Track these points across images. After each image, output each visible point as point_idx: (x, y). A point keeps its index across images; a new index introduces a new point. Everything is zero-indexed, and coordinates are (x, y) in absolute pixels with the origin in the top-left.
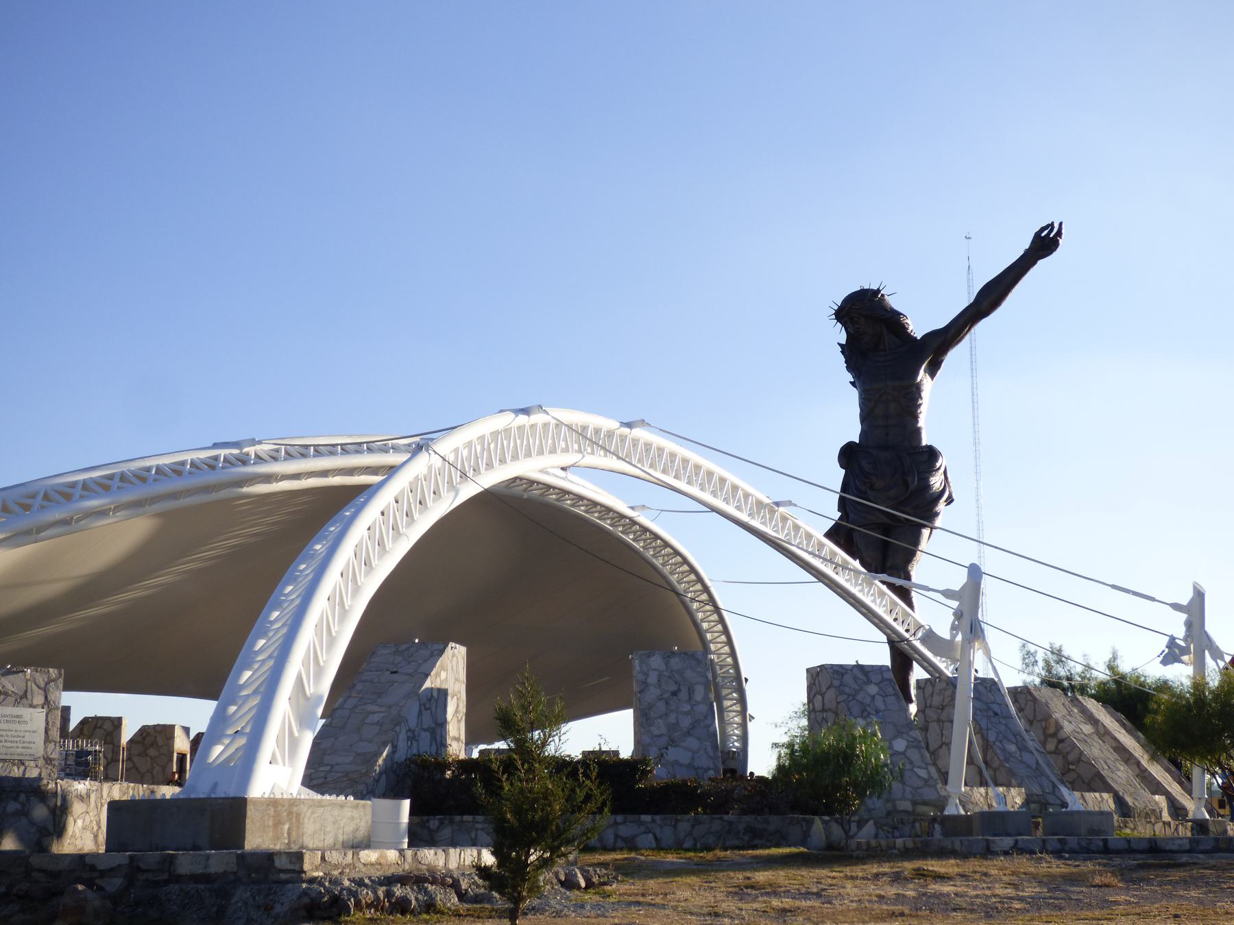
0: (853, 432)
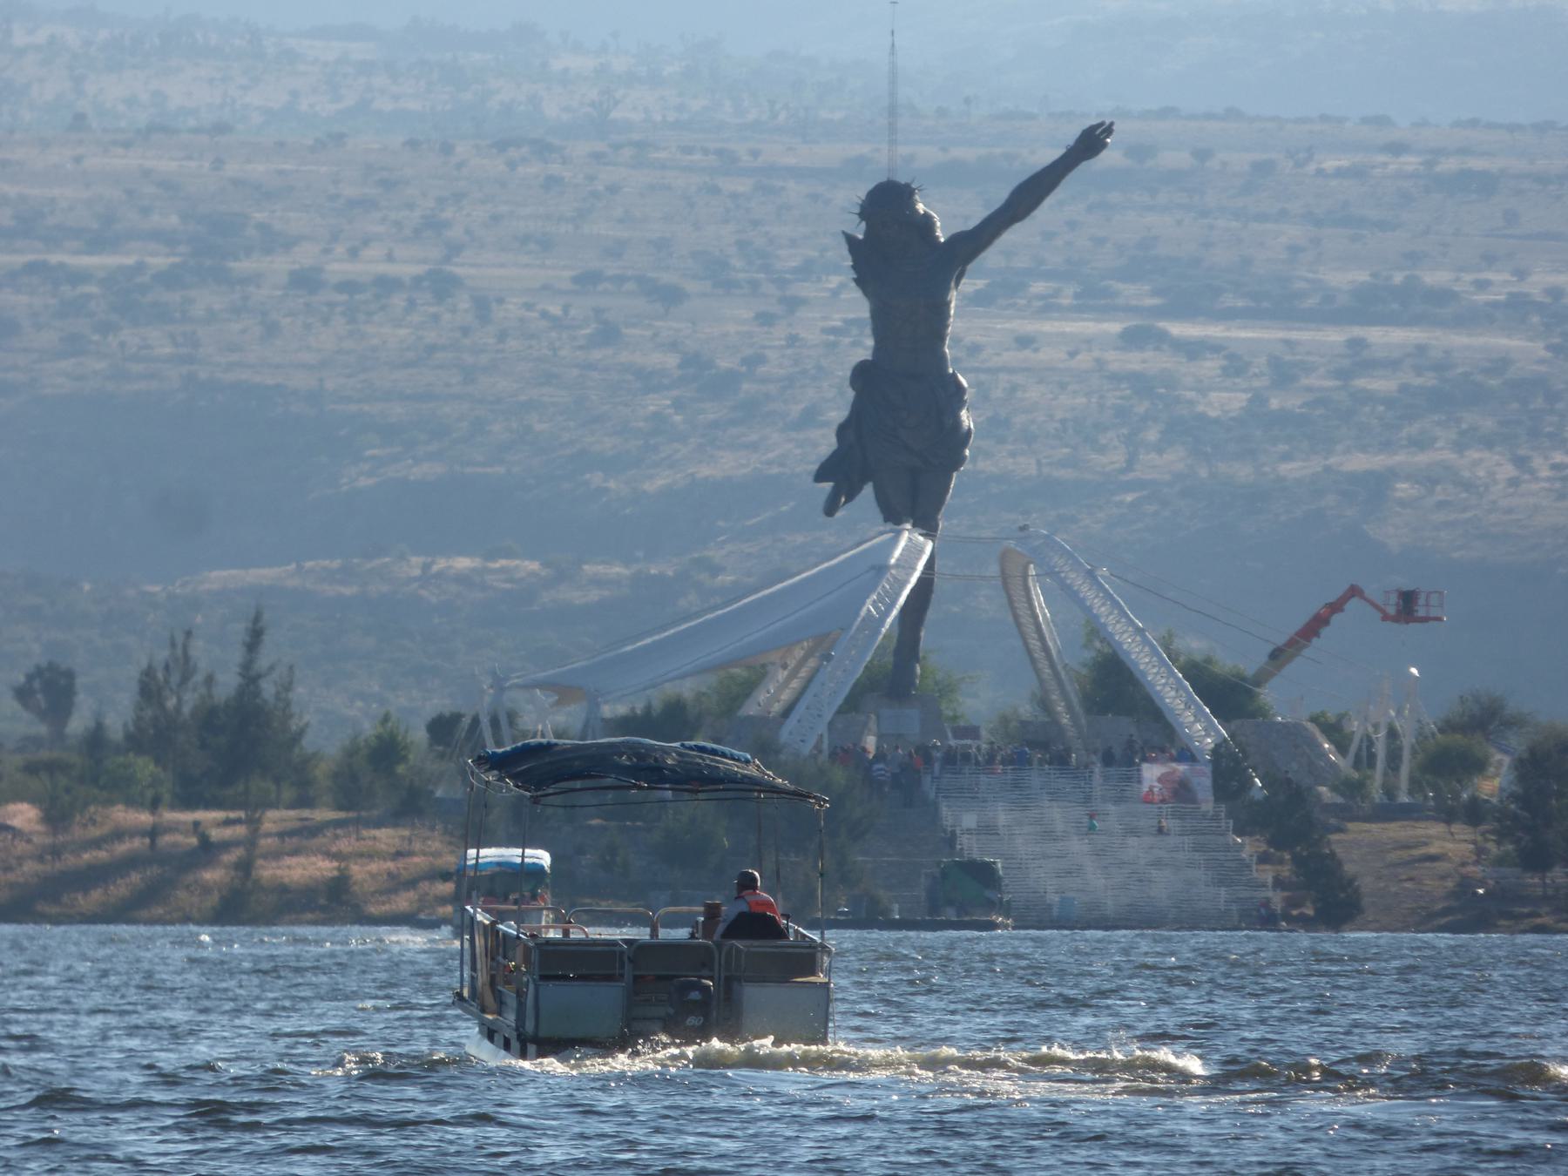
0: (864, 348)
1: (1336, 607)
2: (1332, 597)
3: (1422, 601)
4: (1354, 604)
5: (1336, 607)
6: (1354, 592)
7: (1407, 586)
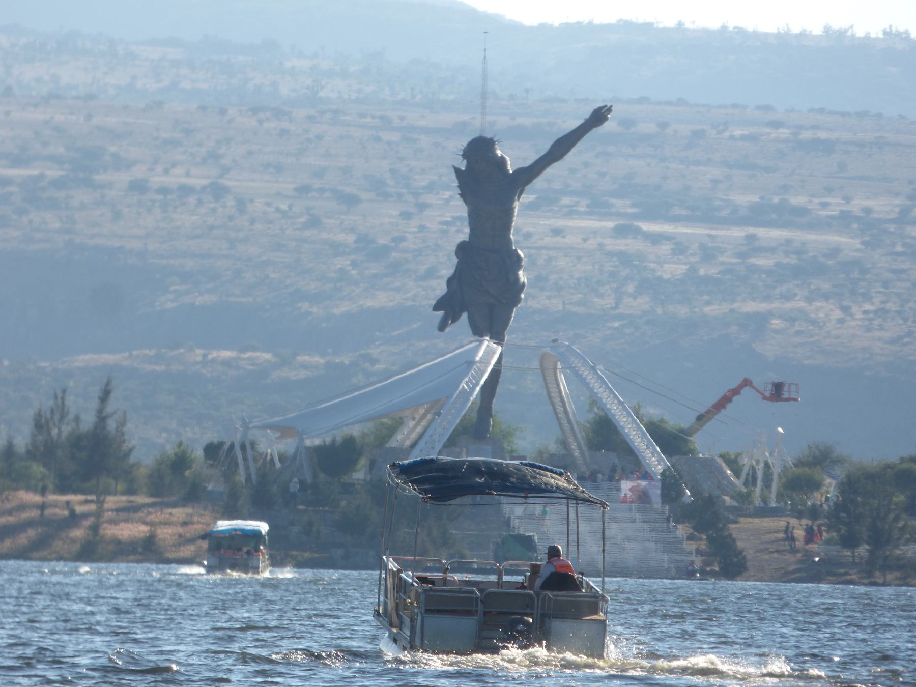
1: (736, 392)
2: (733, 386)
3: (786, 388)
5: (736, 392)
6: (747, 383)
7: (777, 379)
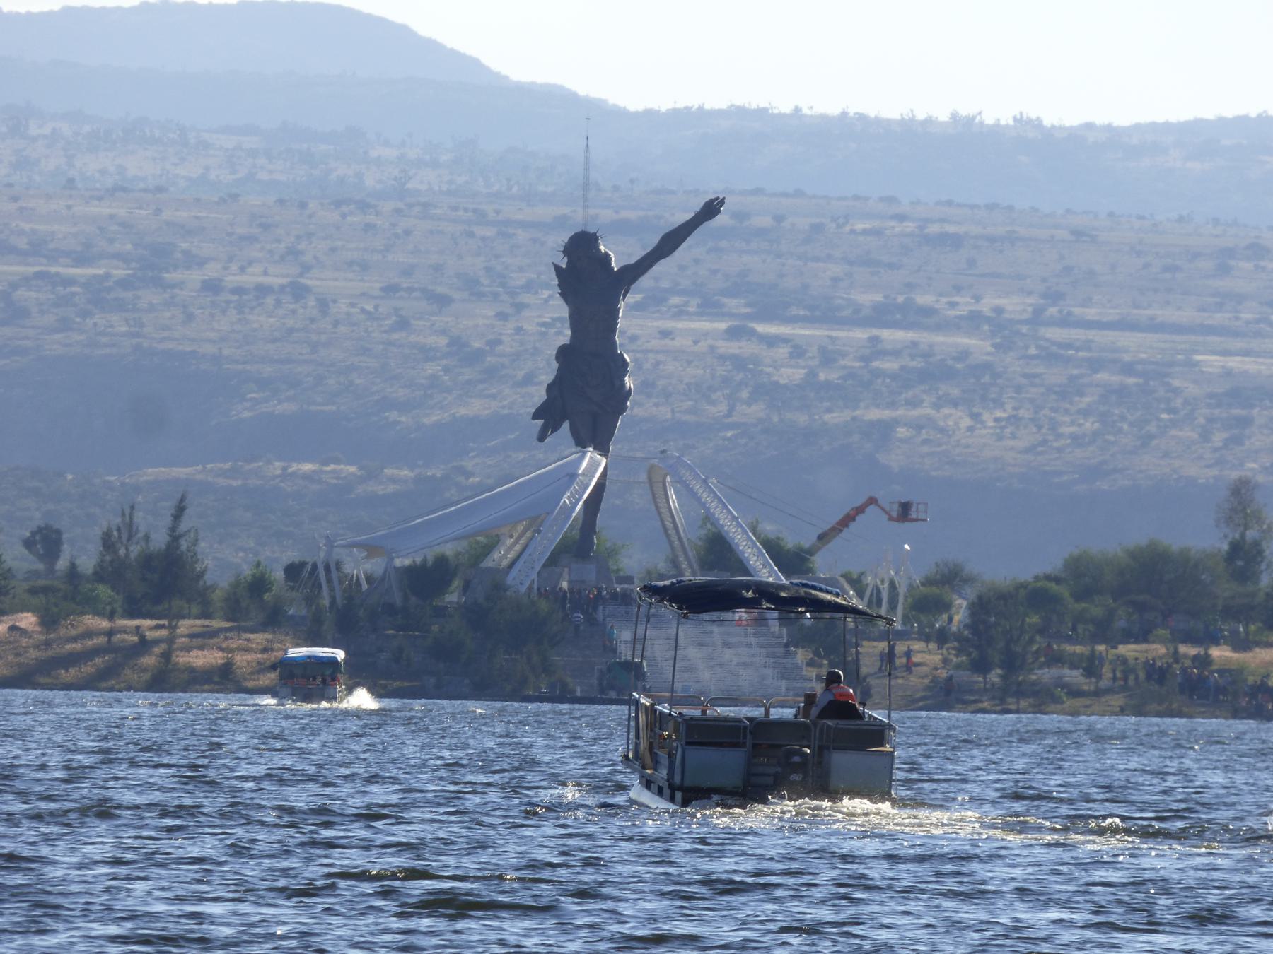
1: (860, 510)
4: (871, 509)
5: (860, 510)
6: (872, 501)
